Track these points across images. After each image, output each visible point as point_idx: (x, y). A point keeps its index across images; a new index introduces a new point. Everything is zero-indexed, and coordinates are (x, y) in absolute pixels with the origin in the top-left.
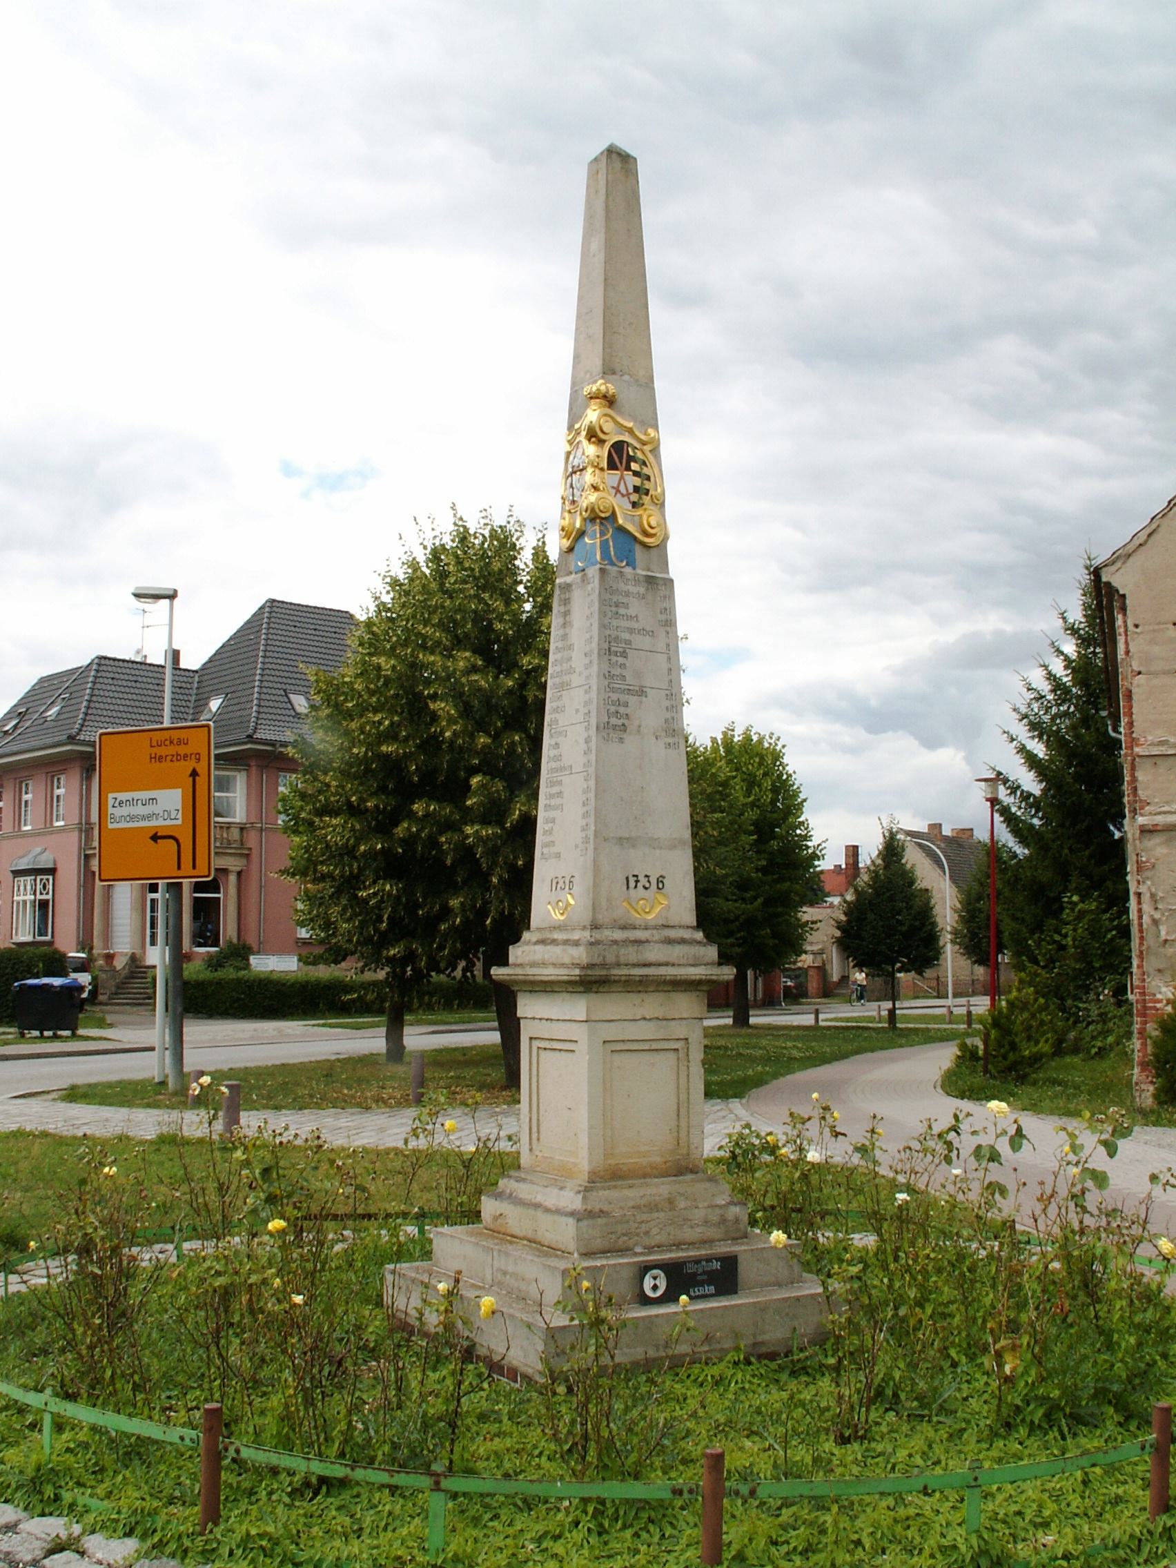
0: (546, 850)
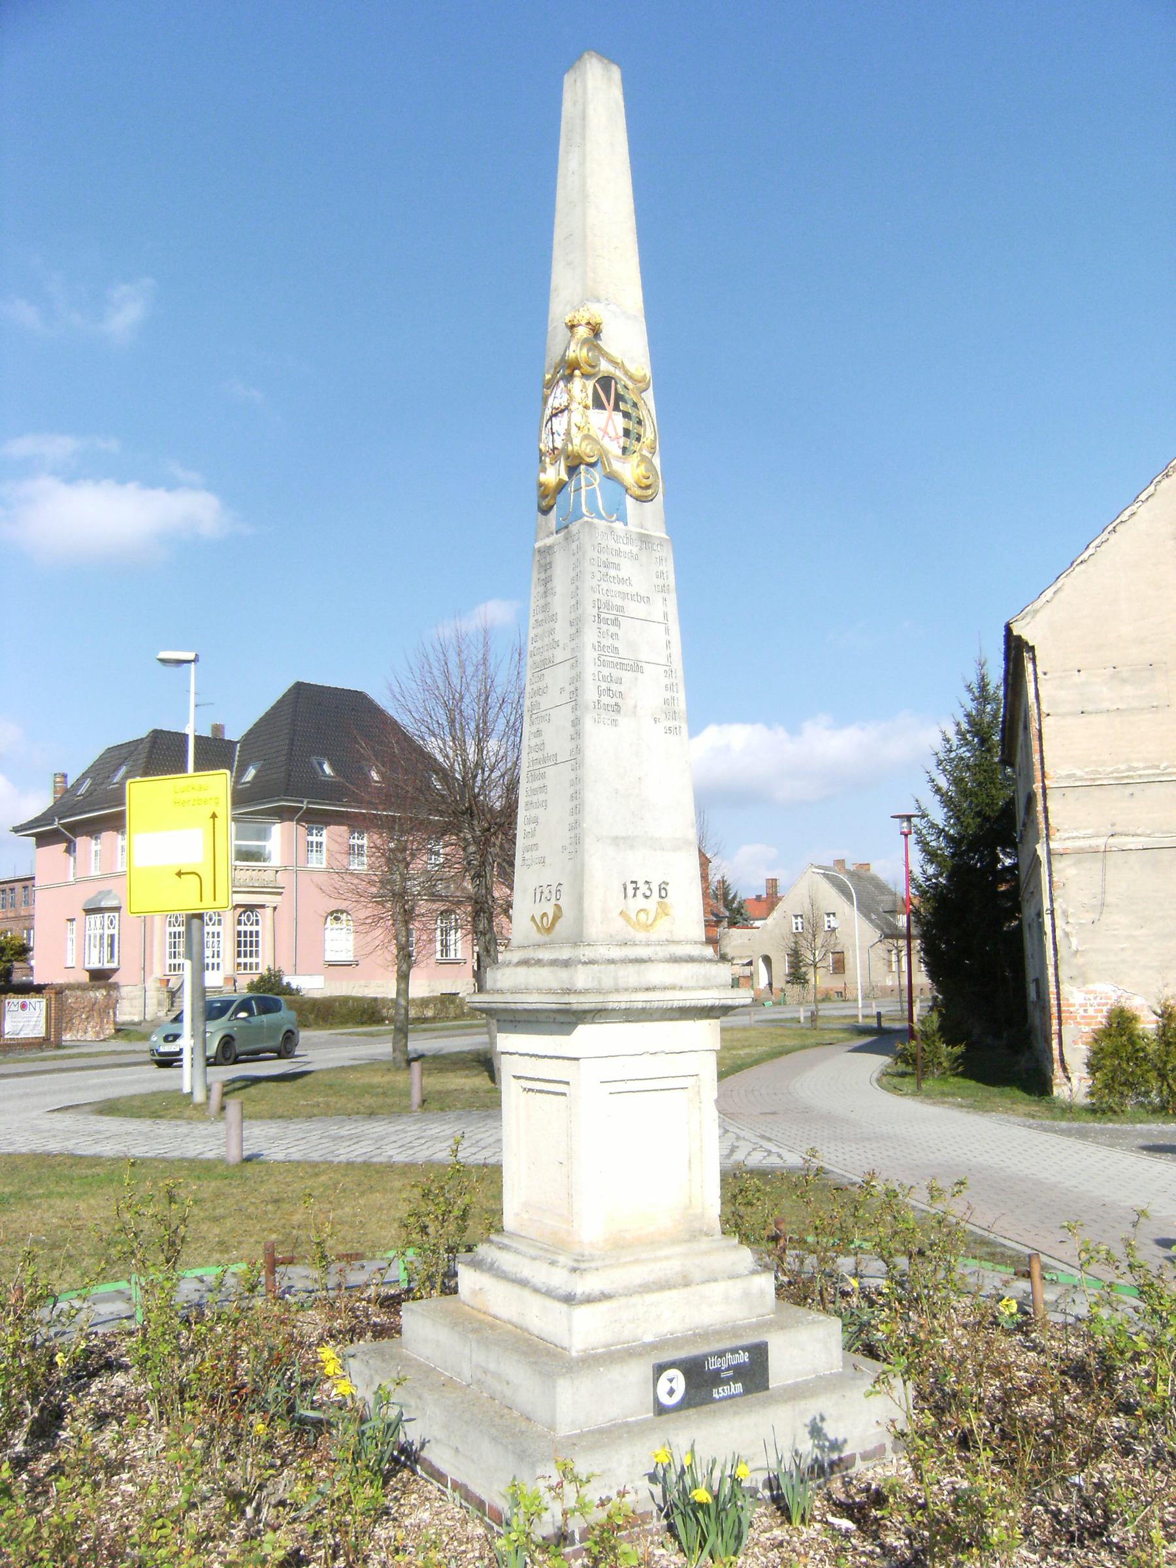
0: (527, 855)
